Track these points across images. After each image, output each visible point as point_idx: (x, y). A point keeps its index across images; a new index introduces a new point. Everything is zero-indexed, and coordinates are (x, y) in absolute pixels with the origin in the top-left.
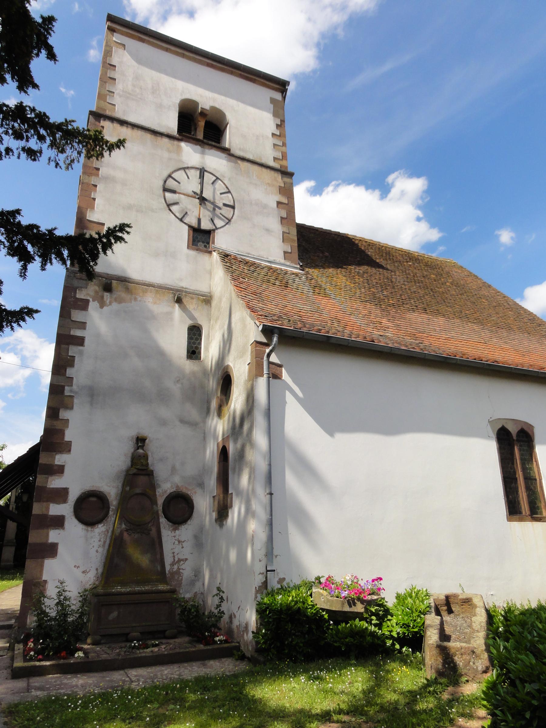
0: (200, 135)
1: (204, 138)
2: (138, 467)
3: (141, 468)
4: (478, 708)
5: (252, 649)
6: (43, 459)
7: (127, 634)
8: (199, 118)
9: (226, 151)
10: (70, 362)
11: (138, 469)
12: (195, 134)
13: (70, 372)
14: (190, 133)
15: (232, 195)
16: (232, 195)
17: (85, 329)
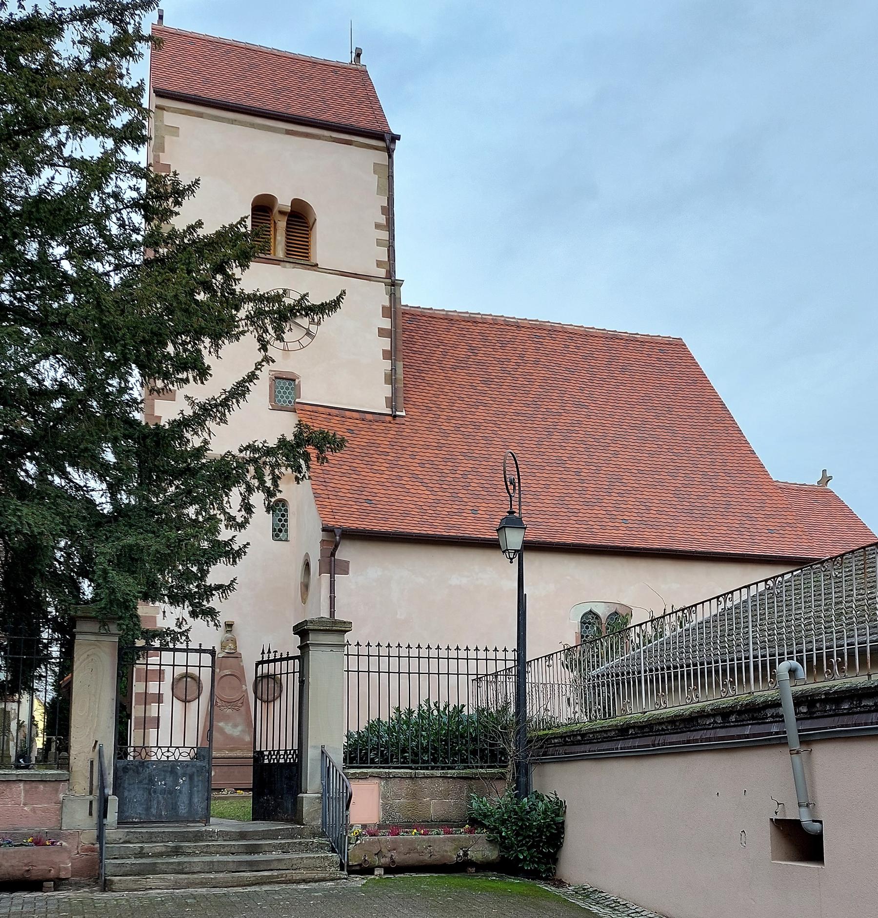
2: (226, 651)
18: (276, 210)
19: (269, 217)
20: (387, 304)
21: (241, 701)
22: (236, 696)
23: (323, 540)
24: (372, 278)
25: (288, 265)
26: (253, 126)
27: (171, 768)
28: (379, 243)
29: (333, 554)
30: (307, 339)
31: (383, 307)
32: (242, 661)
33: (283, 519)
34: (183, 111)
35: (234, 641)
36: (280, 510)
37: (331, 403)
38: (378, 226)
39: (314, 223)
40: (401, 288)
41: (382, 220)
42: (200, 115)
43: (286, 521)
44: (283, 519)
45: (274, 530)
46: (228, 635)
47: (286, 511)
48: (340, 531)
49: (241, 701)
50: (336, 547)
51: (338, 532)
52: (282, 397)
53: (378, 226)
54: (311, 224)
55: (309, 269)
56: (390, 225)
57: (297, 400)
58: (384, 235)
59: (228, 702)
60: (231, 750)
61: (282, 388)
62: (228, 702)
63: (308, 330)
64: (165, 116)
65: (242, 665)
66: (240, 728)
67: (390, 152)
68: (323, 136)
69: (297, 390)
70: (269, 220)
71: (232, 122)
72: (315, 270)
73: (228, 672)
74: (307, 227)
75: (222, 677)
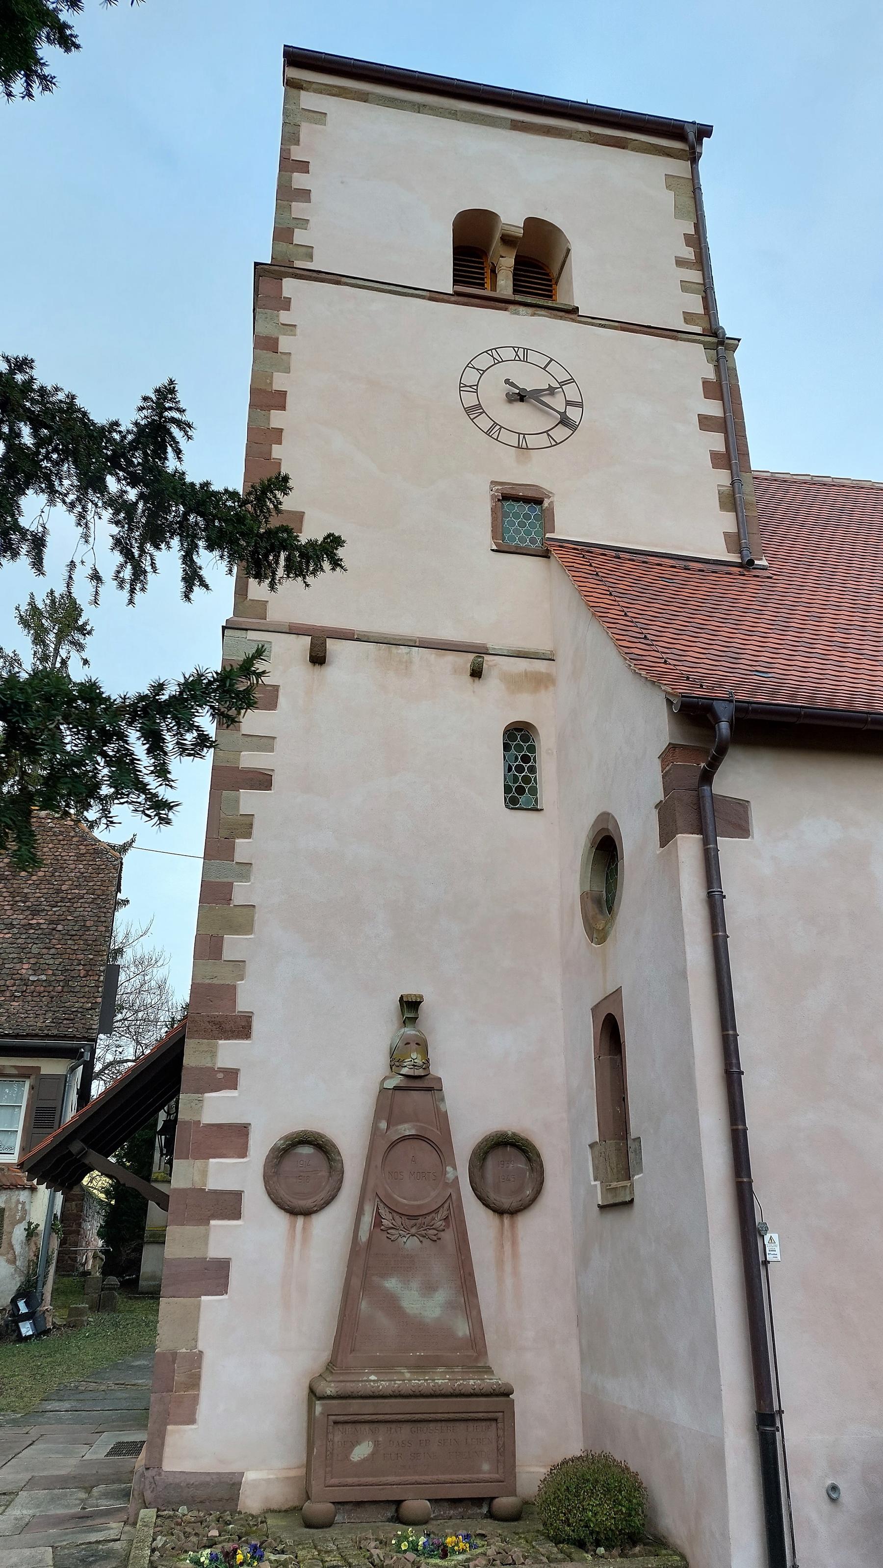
0: (505, 285)
1: (515, 291)
2: (405, 1071)
3: (411, 1073)
4: (43, 1286)
5: (322, 1413)
6: (192, 1058)
7: (399, 1503)
8: (502, 250)
9: (571, 312)
10: (245, 827)
11: (407, 1076)
12: (494, 287)
13: (243, 848)
14: (482, 286)
15: (566, 399)
16: (566, 399)
17: (272, 750)
18: (497, 236)
19: (482, 263)
20: (711, 376)
21: (443, 1213)
22: (430, 1198)
23: (672, 748)
24: (680, 335)
25: (522, 309)
26: (454, 115)
27: (21, 491)
28: (686, 286)
29: (707, 777)
30: (561, 433)
31: (706, 383)
32: (443, 1099)
33: (526, 766)
34: (335, 91)
35: (422, 1045)
36: (519, 748)
37: (617, 541)
38: (681, 263)
39: (560, 274)
40: (736, 355)
41: (689, 253)
42: (363, 97)
43: (532, 770)
44: (526, 766)
45: (507, 789)
46: (409, 1031)
47: (532, 749)
48: (732, 706)
49: (443, 1213)
50: (714, 764)
51: (724, 712)
52: (517, 532)
53: (681, 263)
54: (555, 274)
55: (561, 318)
56: (702, 261)
57: (548, 535)
58: (695, 276)
59: (411, 1217)
60: (421, 1366)
61: (516, 515)
62: (411, 1217)
63: (563, 415)
64: (301, 98)
65: (443, 1110)
66: (441, 1296)
67: (694, 158)
68: (577, 132)
69: (547, 520)
70: (483, 269)
71: (419, 108)
72: (573, 320)
73: (407, 1129)
74: (550, 280)
75: (393, 1145)
